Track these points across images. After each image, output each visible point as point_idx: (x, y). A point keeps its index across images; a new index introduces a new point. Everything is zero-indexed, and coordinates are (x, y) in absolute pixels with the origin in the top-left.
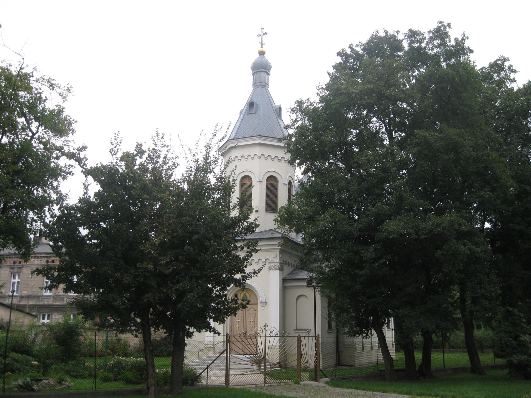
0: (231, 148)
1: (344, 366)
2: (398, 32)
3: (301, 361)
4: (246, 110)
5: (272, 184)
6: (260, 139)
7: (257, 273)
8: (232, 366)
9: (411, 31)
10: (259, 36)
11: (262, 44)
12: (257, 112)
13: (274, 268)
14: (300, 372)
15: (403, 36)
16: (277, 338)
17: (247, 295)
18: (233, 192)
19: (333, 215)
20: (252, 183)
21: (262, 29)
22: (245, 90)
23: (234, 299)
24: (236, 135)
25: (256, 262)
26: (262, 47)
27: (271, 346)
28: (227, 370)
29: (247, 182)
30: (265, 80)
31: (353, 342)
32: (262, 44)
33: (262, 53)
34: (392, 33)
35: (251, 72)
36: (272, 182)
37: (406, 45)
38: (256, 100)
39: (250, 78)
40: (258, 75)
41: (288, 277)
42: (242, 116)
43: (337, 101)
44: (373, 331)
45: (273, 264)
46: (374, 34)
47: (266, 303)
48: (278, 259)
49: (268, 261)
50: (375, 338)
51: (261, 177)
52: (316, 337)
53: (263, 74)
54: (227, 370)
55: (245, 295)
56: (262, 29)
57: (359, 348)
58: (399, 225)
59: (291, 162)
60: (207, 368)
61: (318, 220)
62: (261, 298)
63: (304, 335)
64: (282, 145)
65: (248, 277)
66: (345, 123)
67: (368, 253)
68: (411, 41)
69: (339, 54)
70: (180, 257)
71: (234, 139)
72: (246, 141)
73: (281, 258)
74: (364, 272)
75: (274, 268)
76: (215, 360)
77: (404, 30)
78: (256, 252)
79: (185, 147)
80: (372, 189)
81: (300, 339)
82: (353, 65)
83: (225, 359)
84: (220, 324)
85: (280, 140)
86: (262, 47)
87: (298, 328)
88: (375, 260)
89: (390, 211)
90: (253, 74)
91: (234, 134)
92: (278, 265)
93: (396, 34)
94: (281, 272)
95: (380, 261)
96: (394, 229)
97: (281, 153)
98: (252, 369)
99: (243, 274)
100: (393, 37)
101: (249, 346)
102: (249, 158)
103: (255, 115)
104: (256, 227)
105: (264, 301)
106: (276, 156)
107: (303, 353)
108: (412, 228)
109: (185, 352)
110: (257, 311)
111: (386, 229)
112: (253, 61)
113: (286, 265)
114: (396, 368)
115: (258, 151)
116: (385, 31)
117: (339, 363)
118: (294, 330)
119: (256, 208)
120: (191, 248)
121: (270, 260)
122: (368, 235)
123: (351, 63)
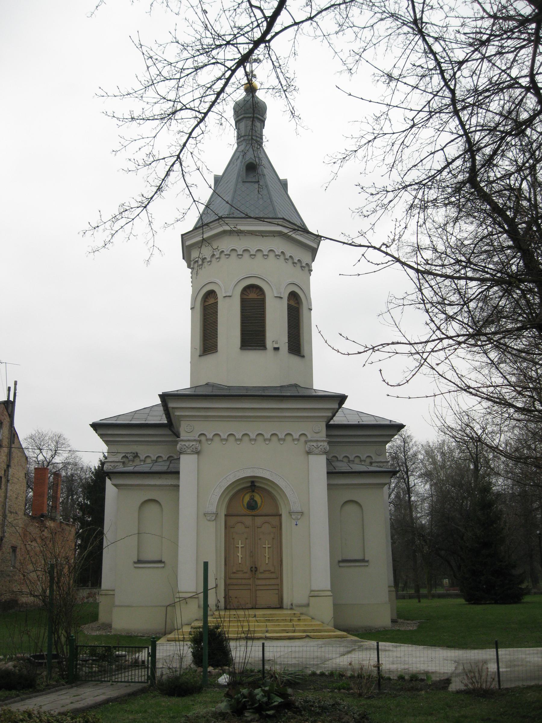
13: (317, 451)
17: (257, 498)
36: (253, 295)
45: (315, 444)
55: (252, 498)
118: (135, 563)
121: (309, 437)
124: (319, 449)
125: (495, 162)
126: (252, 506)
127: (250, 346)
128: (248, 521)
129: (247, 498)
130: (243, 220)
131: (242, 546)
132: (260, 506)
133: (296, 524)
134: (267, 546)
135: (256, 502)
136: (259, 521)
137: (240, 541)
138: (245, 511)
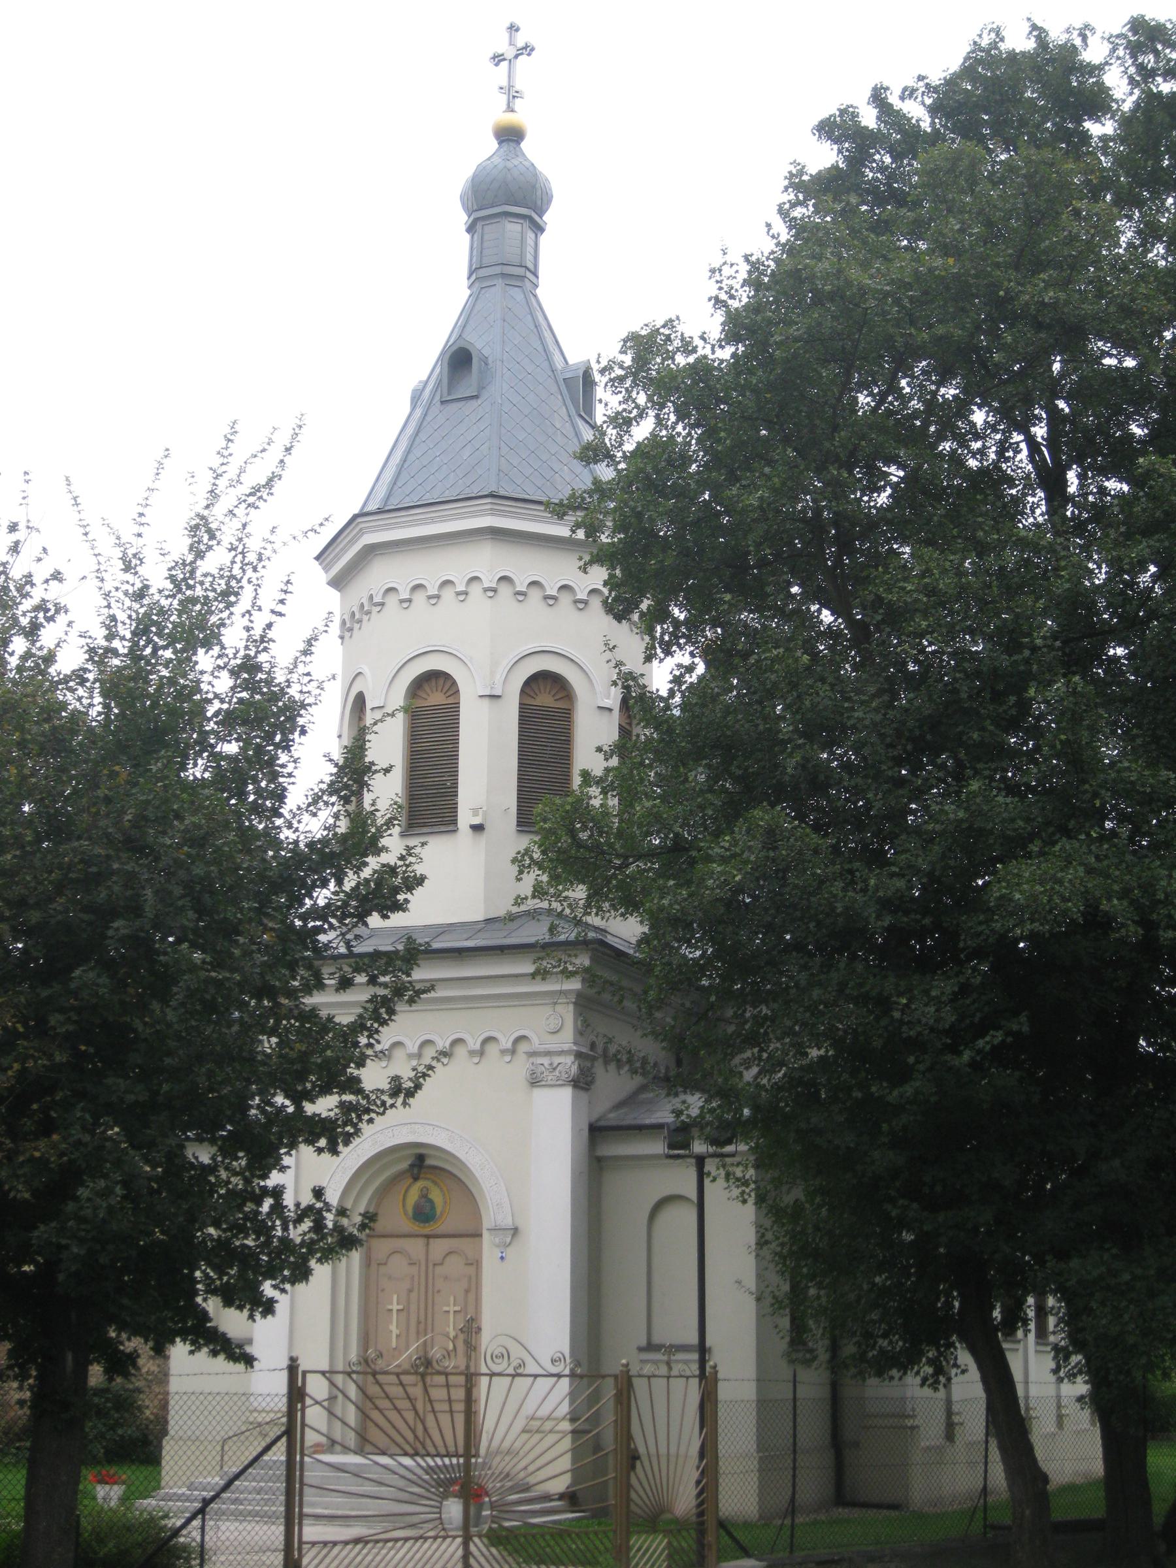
0: (371, 552)
1: (879, 1506)
2: (1085, 32)
3: (629, 1486)
4: (439, 383)
5: (545, 706)
6: (493, 513)
7: (410, 1094)
8: (313, 1503)
9: (1138, 24)
10: (498, 59)
11: (512, 94)
12: (485, 395)
13: (550, 1078)
14: (629, 1534)
15: (1106, 48)
16: (565, 1383)
17: (436, 1195)
18: (303, 732)
19: (772, 836)
20: (456, 707)
21: (513, 28)
22: (435, 295)
23: (310, 1208)
24: (389, 495)
25: (472, 1053)
26: (510, 109)
27: (528, 1419)
28: (292, 1518)
29: (435, 698)
30: (522, 255)
31: (903, 1399)
32: (512, 94)
33: (510, 136)
34: (1062, 39)
35: (462, 218)
36: (544, 699)
37: (1118, 83)
38: (478, 342)
39: (454, 246)
40: (491, 231)
41: (613, 1118)
42: (419, 412)
43: (793, 331)
44: (964, 1357)
45: (546, 1061)
46: (985, 43)
47: (515, 1231)
48: (567, 1039)
49: (523, 1047)
50: (968, 1386)
51: (499, 677)
52: (702, 1375)
53: (513, 228)
54: (292, 1518)
55: (424, 1195)
56: (513, 28)
57: (931, 1431)
58: (1060, 882)
59: (619, 609)
60: (202, 1511)
61: (709, 859)
62: (495, 1207)
63: (648, 1369)
64: (563, 531)
65: (368, 1111)
66: (835, 428)
67: (928, 1005)
68: (1141, 68)
69: (827, 129)
70: (54, 1019)
71: (380, 511)
72: (433, 521)
73: (579, 1033)
74: (909, 1090)
75: (550, 1078)
76: (237, 1477)
77: (1114, 21)
78: (411, 1001)
79: (97, 531)
80: (958, 724)
81: (630, 1385)
82: (891, 177)
83: (282, 1471)
84: (251, 1317)
85: (559, 511)
86: (510, 109)
87: (656, 1340)
88: (957, 1038)
89: (1028, 820)
90: (471, 229)
91: (382, 492)
92: (569, 1064)
93: (1078, 42)
94: (584, 1096)
95: (980, 1043)
96: (1034, 897)
97: (562, 570)
98: (415, 1519)
99: (348, 1097)
100: (1070, 51)
101: (392, 1415)
102: (448, 594)
103: (474, 403)
104: (410, 889)
105: (508, 1222)
106: (564, 587)
107: (642, 1450)
108: (1125, 894)
109: (1041, 1464)
110: (476, 1264)
111: (1002, 897)
112: (468, 172)
113: (606, 1063)
114: (1057, 1515)
115: (486, 562)
116: (1034, 27)
117: (842, 1494)
118: (641, 1349)
119: (475, 812)
120: (104, 980)
121: (536, 1044)
122: (931, 932)
123: (882, 169)
124: (557, 1073)
125: (790, 190)
126: (424, 1214)
127: (425, 825)
128: (415, 1247)
129: (414, 1196)
130: (519, 504)
131: (401, 1307)
132: (442, 1214)
133: (502, 1258)
134: (452, 1309)
135: (431, 1201)
136: (439, 1247)
137: (395, 1297)
138: (408, 1226)
